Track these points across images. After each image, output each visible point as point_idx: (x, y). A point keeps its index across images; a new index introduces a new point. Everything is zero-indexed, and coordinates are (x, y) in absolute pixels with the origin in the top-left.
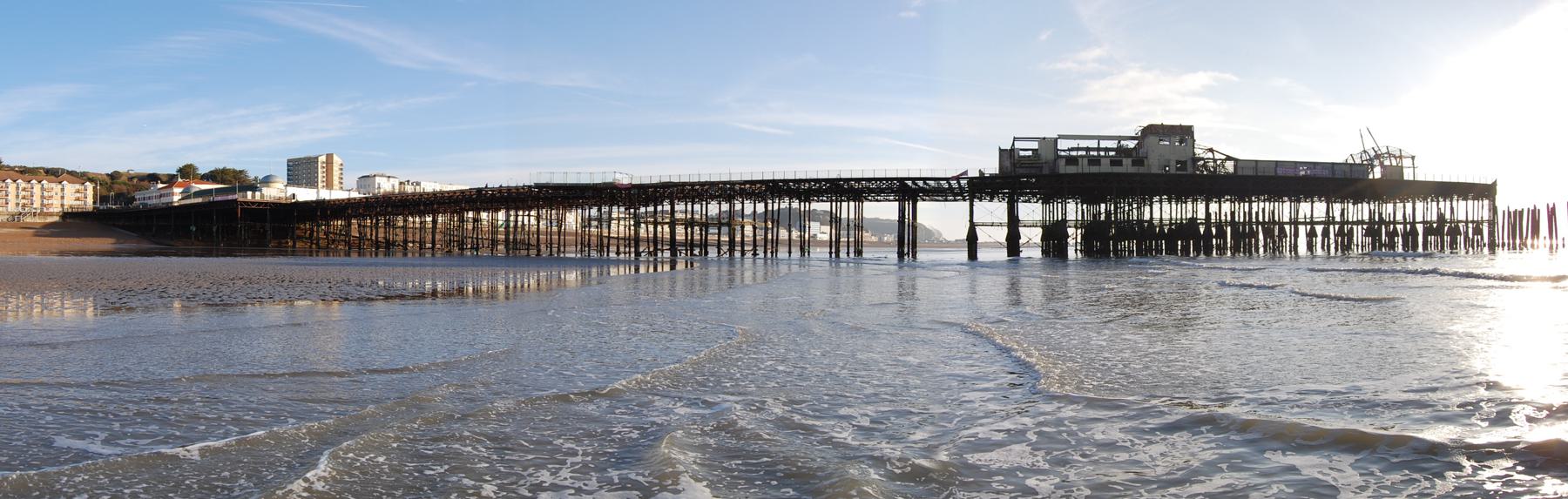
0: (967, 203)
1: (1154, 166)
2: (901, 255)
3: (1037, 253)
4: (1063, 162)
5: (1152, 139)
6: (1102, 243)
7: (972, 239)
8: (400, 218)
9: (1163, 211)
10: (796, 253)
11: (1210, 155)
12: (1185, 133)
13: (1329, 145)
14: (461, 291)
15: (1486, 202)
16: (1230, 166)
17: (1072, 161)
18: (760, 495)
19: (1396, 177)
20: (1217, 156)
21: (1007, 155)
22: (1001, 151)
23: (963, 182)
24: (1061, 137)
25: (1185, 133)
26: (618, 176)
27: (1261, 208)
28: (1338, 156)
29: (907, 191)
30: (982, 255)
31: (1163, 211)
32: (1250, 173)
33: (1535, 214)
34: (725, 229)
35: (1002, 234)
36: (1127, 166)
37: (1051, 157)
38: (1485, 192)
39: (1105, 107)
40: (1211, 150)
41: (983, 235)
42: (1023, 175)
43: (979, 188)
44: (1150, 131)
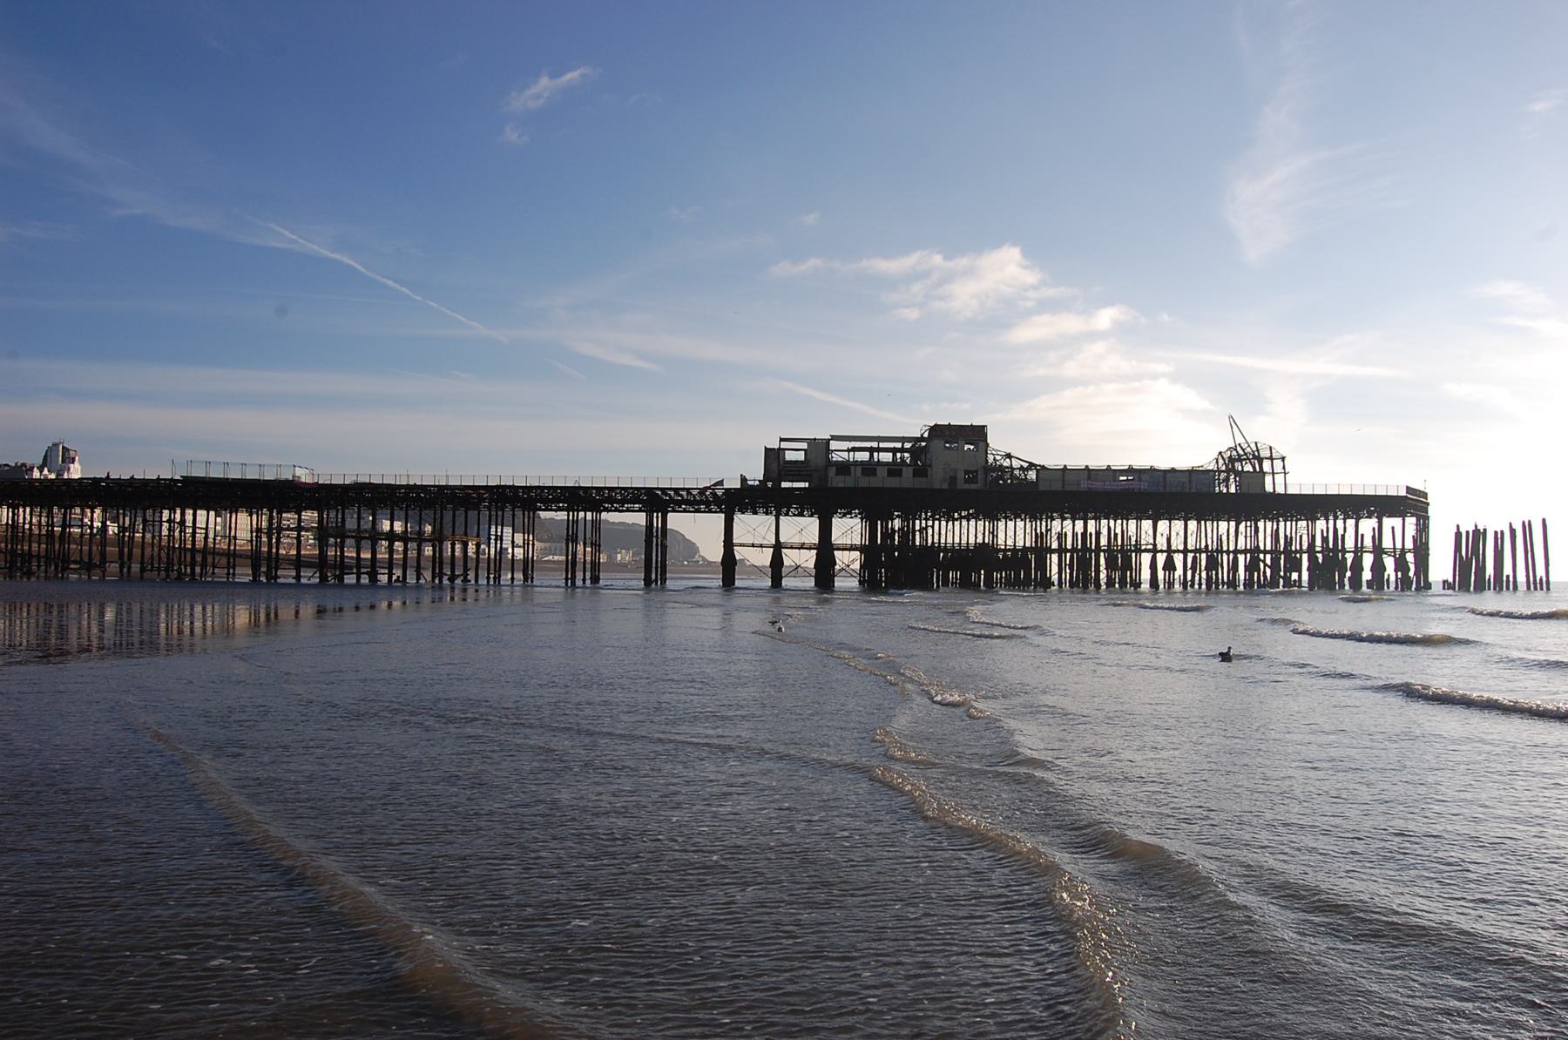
0: (720, 518)
1: (937, 479)
2: (648, 582)
3: (854, 583)
4: (833, 470)
5: (938, 444)
6: (896, 568)
7: (777, 561)
8: (78, 510)
9: (962, 532)
10: (519, 576)
11: (1006, 463)
12: (977, 434)
13: (1188, 446)
14: (341, 610)
15: (1411, 521)
16: (1032, 475)
17: (844, 467)
18: (1546, 1029)
19: (1258, 491)
20: (1016, 464)
21: (773, 456)
22: (768, 452)
23: (720, 493)
24: (834, 438)
25: (977, 434)
26: (299, 472)
27: (1106, 529)
28: (1183, 462)
29: (656, 501)
30: (786, 582)
31: (962, 532)
32: (1057, 487)
33: (1527, 528)
34: (412, 545)
35: (808, 559)
36: (907, 480)
37: (821, 462)
38: (1412, 505)
39: (875, 407)
40: (1009, 456)
41: (790, 558)
42: (802, 481)
43: (731, 501)
44: (935, 430)
